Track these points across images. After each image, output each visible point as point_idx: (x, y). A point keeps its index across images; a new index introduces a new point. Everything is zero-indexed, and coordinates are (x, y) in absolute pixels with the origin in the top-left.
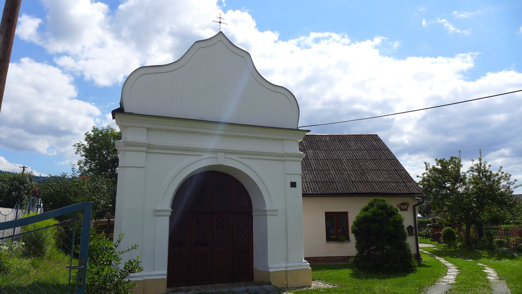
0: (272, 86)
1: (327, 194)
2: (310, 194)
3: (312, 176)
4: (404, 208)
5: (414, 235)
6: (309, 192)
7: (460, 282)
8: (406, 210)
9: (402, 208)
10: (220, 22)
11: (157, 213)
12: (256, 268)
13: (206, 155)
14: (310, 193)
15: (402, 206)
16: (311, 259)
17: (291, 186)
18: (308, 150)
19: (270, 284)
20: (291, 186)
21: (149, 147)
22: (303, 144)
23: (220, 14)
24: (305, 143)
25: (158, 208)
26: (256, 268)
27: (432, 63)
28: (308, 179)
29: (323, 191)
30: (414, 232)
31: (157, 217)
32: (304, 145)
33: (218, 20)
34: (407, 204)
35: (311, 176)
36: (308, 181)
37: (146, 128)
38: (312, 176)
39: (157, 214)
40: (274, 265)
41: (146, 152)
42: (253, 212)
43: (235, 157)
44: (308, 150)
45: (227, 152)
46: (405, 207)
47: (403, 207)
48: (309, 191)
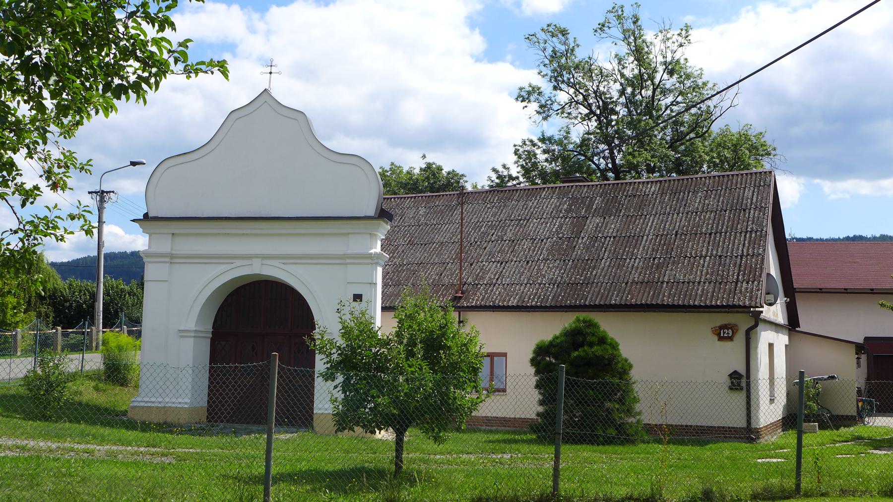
0: (335, 155)
4: (725, 335)
5: (742, 389)
8: (730, 339)
9: (722, 335)
10: (271, 73)
11: (182, 334)
13: (239, 263)
15: (722, 331)
17: (355, 300)
20: (355, 300)
21: (172, 256)
25: (182, 328)
27: (88, 206)
30: (744, 384)
31: (182, 339)
34: (734, 328)
37: (169, 233)
39: (181, 334)
40: (320, 406)
41: (171, 263)
43: (276, 263)
45: (264, 257)
46: (728, 333)
47: (724, 333)
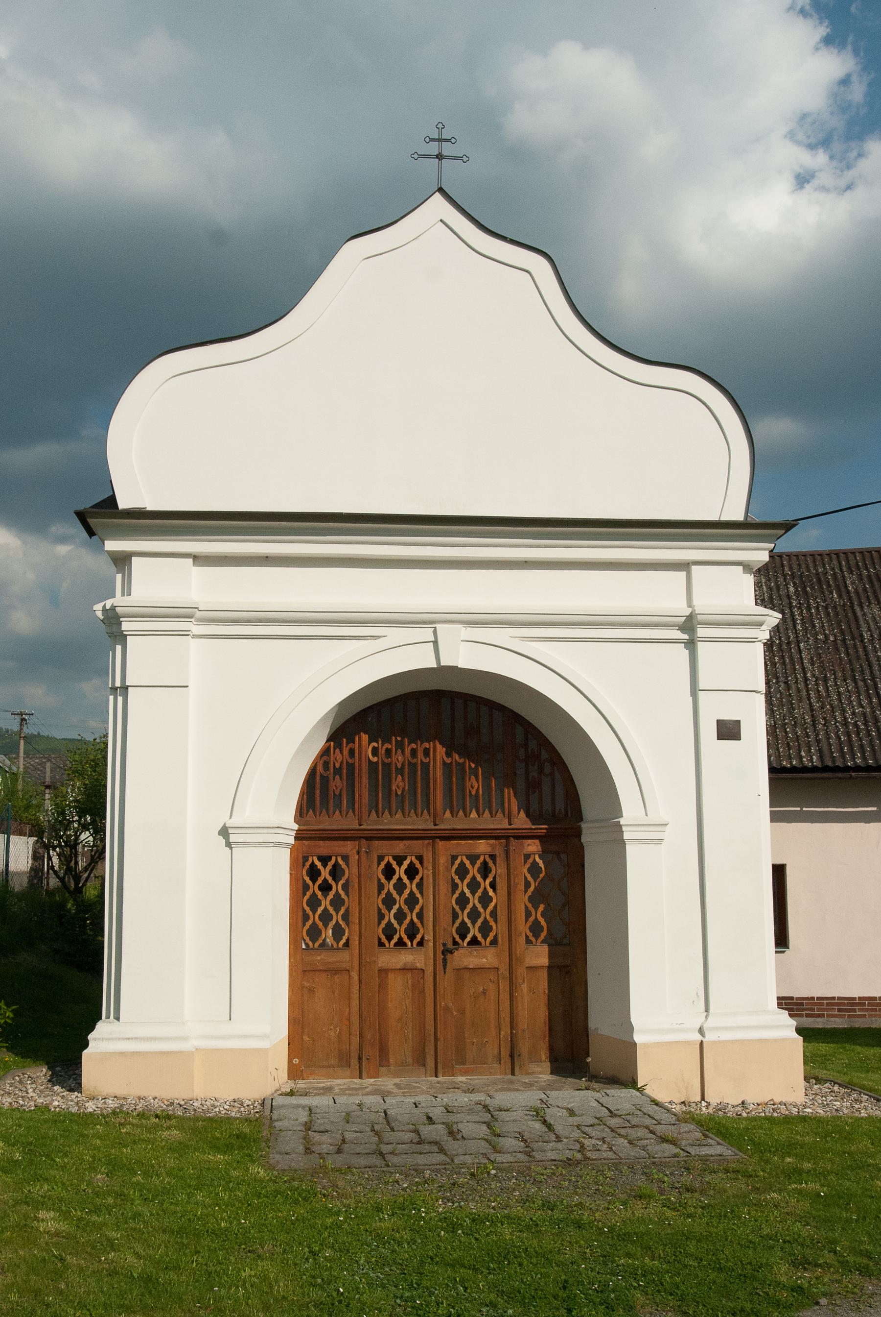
1: (838, 766)
2: (857, 768)
3: (871, 702)
6: (853, 759)
7: (83, 1268)
12: (597, 1029)
14: (856, 763)
16: (802, 1004)
18: (862, 608)
19: (632, 1083)
22: (846, 586)
23: (440, 126)
24: (853, 583)
26: (597, 1029)
28: (854, 713)
29: (833, 759)
32: (848, 592)
33: (433, 149)
35: (865, 702)
36: (852, 719)
38: (871, 702)
42: (584, 832)
44: (862, 608)
48: (853, 755)
